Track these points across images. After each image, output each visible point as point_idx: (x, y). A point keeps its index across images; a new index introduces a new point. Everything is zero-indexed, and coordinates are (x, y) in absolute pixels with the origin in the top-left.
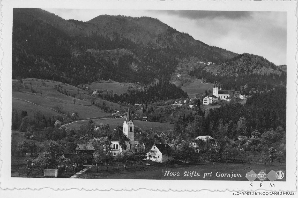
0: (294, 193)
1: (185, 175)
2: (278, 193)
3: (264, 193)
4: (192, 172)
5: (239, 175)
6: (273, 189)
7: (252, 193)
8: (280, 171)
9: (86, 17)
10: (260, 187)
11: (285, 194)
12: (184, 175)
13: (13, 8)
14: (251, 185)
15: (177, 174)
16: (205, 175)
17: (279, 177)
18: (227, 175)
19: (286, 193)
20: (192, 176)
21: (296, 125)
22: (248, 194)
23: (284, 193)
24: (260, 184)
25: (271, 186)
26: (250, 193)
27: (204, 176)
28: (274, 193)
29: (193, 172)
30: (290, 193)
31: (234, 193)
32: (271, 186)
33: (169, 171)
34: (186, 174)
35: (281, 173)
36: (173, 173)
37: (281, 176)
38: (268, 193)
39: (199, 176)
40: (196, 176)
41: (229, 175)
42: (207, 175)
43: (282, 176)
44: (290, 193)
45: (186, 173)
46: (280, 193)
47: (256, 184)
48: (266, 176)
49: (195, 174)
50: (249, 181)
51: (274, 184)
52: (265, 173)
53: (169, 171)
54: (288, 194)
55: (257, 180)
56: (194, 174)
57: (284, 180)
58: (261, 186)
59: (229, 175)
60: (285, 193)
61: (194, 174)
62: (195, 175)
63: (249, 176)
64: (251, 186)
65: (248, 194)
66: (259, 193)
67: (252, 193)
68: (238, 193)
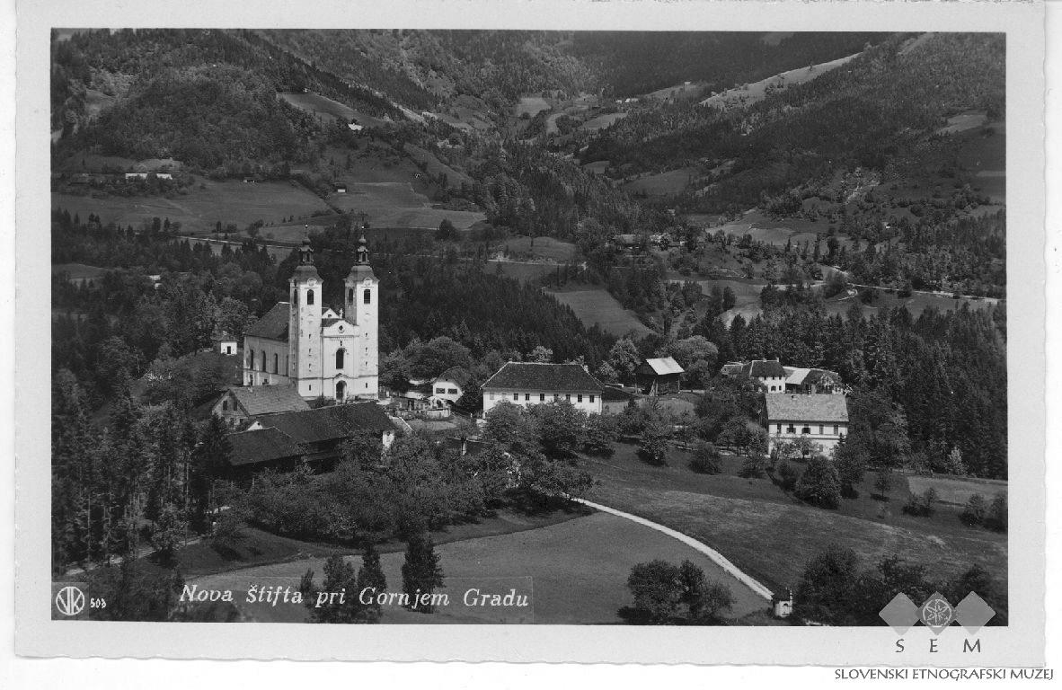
0: (1049, 672)
1: (251, 599)
2: (992, 673)
3: (944, 674)
4: (275, 590)
5: (441, 596)
6: (973, 660)
7: (903, 674)
8: (73, 588)
10: (931, 651)
11: (1017, 677)
12: (248, 600)
15: (223, 594)
16: (320, 597)
17: (68, 609)
18: (396, 600)
19: (1021, 672)
22: (889, 676)
23: (1012, 672)
24: (932, 641)
25: (970, 647)
26: (894, 673)
27: (319, 601)
29: (280, 588)
30: (1036, 673)
31: (838, 672)
32: (970, 647)
33: (195, 587)
34: (253, 596)
35: (76, 593)
36: (210, 593)
37: (74, 604)
38: (959, 672)
39: (300, 601)
40: (290, 601)
41: (521, 602)
42: (327, 598)
43: (80, 604)
44: (1036, 673)
45: (253, 593)
46: (1001, 674)
47: (917, 637)
49: (286, 596)
50: (887, 625)
51: (978, 643)
52: (946, 604)
53: (195, 587)
54: (1029, 674)
56: (281, 597)
57: (56, 615)
58: (934, 649)
59: (521, 602)
60: (1017, 672)
61: (281, 597)
62: (286, 600)
63: (476, 600)
64: (900, 649)
65: (889, 676)
66: (926, 673)
67: (903, 674)
68: (854, 674)
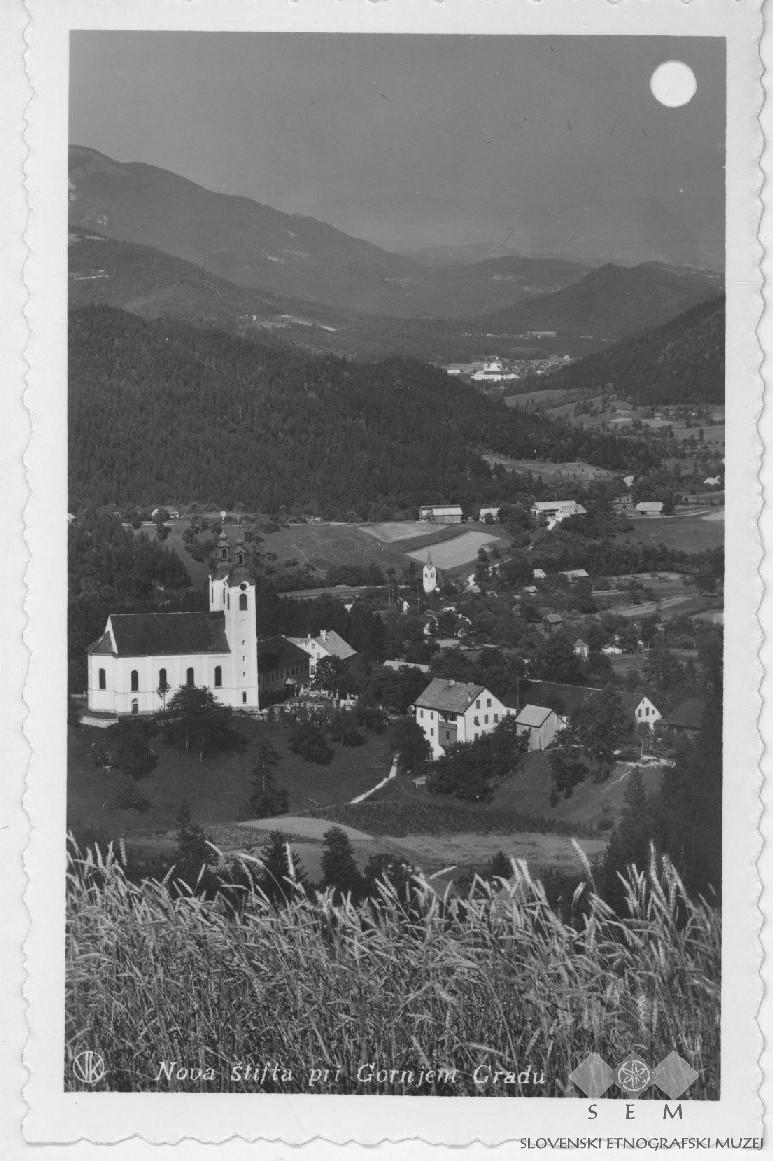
9: (226, 631)
10: (628, 1117)
11: (723, 1146)
13: (82, 43)
14: (591, 1111)
20: (262, 1080)
21: (26, 1102)
25: (670, 1114)
28: (680, 1141)
32: (670, 1114)
38: (659, 1141)
44: (744, 1143)
48: (651, 1074)
51: (679, 1108)
54: (736, 1143)
55: (614, 1093)
58: (631, 1115)
64: (593, 1115)
